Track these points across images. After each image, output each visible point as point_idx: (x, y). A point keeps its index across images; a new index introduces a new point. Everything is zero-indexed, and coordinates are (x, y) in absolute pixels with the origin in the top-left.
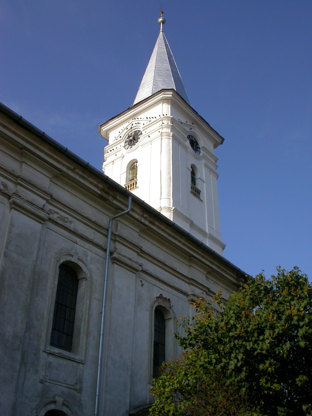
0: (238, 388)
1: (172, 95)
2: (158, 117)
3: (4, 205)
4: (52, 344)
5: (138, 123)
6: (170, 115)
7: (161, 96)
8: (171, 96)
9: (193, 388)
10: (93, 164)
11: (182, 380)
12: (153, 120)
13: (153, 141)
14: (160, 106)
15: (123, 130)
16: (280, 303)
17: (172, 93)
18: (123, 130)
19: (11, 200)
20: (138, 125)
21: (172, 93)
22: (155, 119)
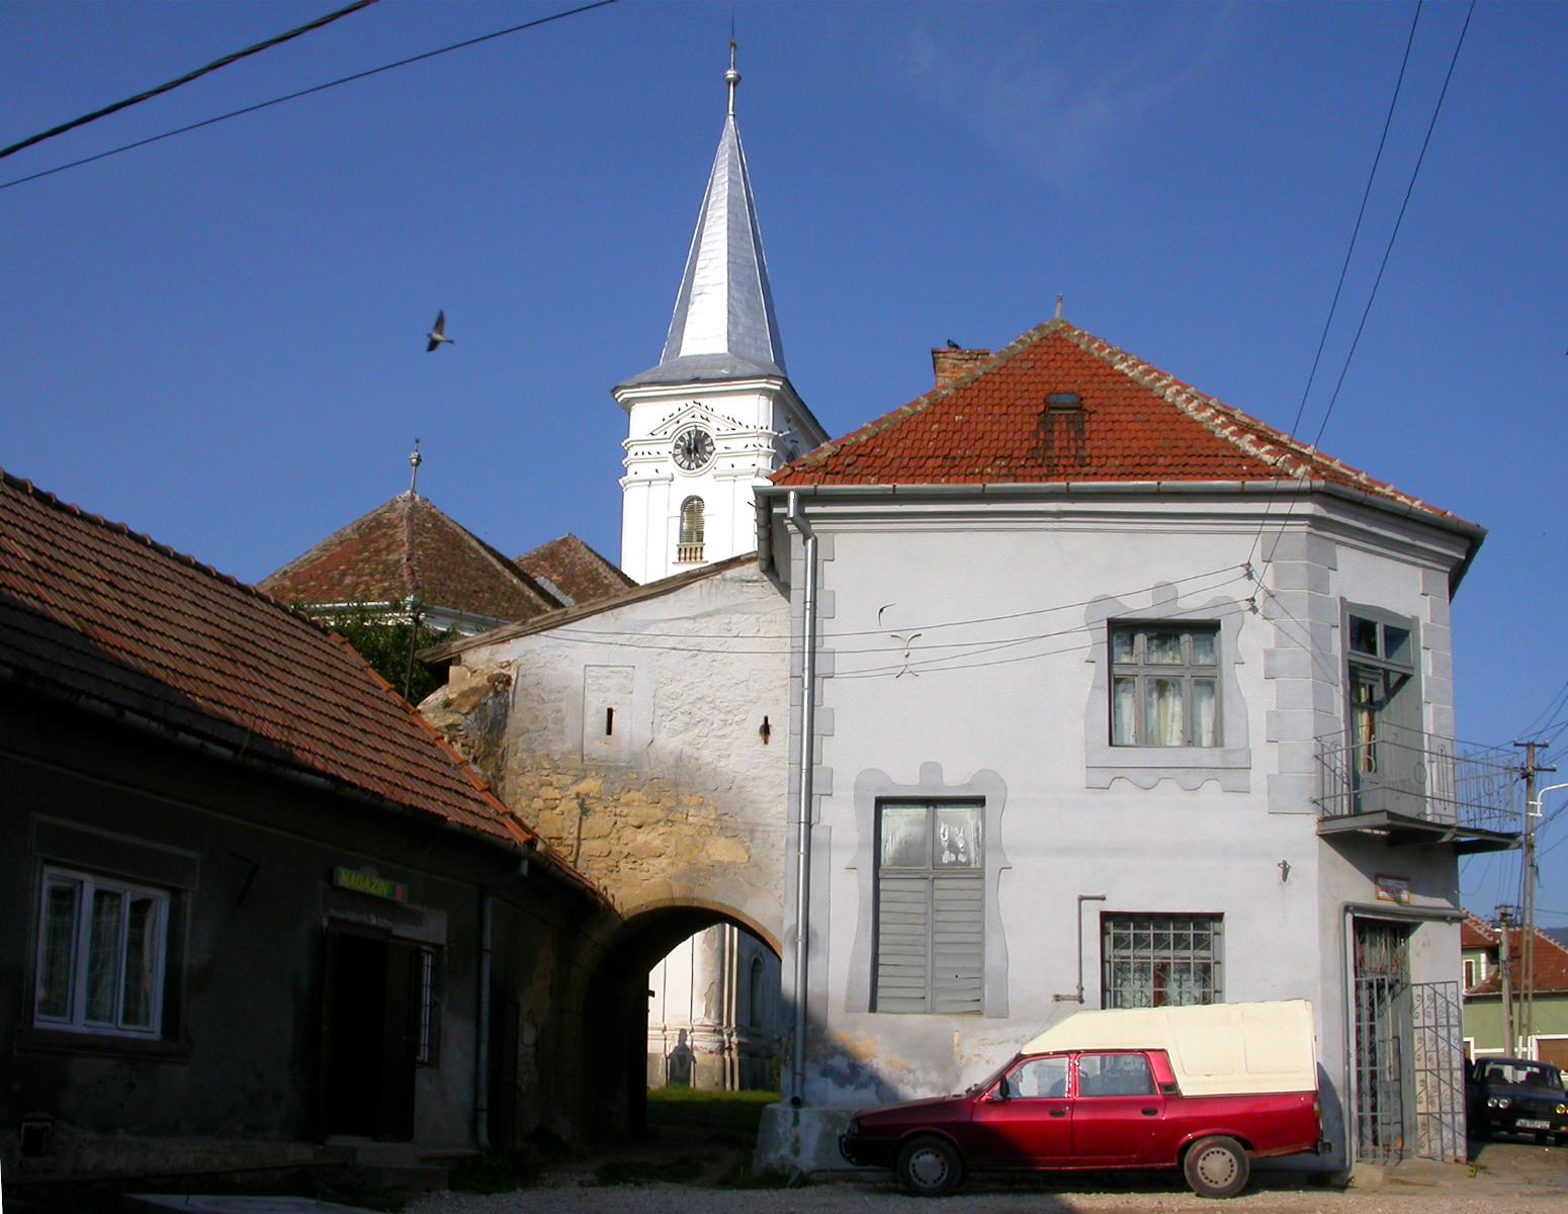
0: (1281, 439)
1: (781, 387)
2: (751, 429)
3: (1512, 857)
4: (87, 1019)
5: (707, 419)
6: (770, 430)
7: (762, 384)
8: (778, 388)
9: (602, 864)
10: (618, 567)
11: (366, 575)
12: (740, 430)
13: (739, 477)
14: (754, 398)
15: (667, 420)
16: (1076, 382)
17: (781, 383)
18: (667, 420)
19: (559, 727)
20: (705, 422)
21: (781, 383)
22: (744, 429)
